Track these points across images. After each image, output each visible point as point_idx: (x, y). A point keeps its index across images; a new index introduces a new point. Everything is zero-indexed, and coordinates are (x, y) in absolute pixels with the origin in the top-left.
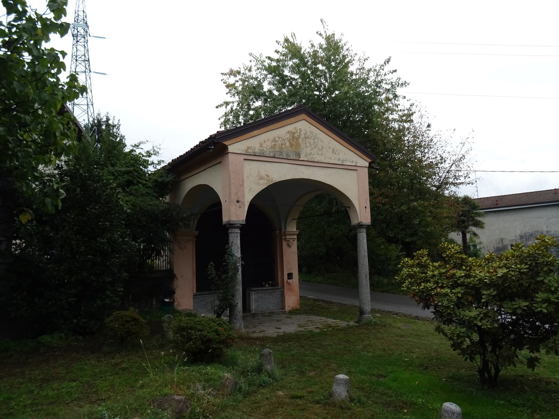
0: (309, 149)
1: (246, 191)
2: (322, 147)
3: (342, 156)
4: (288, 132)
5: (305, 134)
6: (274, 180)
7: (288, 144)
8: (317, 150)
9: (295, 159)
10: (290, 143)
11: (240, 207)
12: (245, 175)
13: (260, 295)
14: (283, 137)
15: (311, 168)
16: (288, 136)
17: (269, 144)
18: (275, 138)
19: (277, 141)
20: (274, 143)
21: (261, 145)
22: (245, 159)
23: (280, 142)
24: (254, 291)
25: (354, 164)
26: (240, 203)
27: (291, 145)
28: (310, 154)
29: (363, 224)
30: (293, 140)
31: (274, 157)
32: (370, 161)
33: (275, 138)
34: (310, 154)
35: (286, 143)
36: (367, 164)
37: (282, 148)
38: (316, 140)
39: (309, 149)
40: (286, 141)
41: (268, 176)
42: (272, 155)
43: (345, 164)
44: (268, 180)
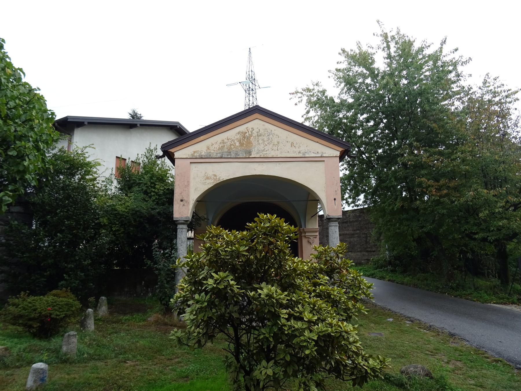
1: (192, 190)
2: (278, 143)
3: (303, 149)
4: (239, 133)
5: (258, 132)
7: (238, 144)
8: (271, 146)
9: (247, 157)
10: (240, 143)
11: (184, 205)
12: (192, 176)
14: (233, 138)
16: (238, 136)
17: (217, 146)
19: (226, 143)
20: (222, 145)
23: (229, 143)
27: (241, 144)
28: (263, 150)
32: (341, 149)
34: (263, 150)
36: (338, 154)
37: (231, 148)
38: (271, 136)
39: (262, 145)
40: (236, 141)
41: (215, 176)
42: (219, 155)
44: (215, 180)
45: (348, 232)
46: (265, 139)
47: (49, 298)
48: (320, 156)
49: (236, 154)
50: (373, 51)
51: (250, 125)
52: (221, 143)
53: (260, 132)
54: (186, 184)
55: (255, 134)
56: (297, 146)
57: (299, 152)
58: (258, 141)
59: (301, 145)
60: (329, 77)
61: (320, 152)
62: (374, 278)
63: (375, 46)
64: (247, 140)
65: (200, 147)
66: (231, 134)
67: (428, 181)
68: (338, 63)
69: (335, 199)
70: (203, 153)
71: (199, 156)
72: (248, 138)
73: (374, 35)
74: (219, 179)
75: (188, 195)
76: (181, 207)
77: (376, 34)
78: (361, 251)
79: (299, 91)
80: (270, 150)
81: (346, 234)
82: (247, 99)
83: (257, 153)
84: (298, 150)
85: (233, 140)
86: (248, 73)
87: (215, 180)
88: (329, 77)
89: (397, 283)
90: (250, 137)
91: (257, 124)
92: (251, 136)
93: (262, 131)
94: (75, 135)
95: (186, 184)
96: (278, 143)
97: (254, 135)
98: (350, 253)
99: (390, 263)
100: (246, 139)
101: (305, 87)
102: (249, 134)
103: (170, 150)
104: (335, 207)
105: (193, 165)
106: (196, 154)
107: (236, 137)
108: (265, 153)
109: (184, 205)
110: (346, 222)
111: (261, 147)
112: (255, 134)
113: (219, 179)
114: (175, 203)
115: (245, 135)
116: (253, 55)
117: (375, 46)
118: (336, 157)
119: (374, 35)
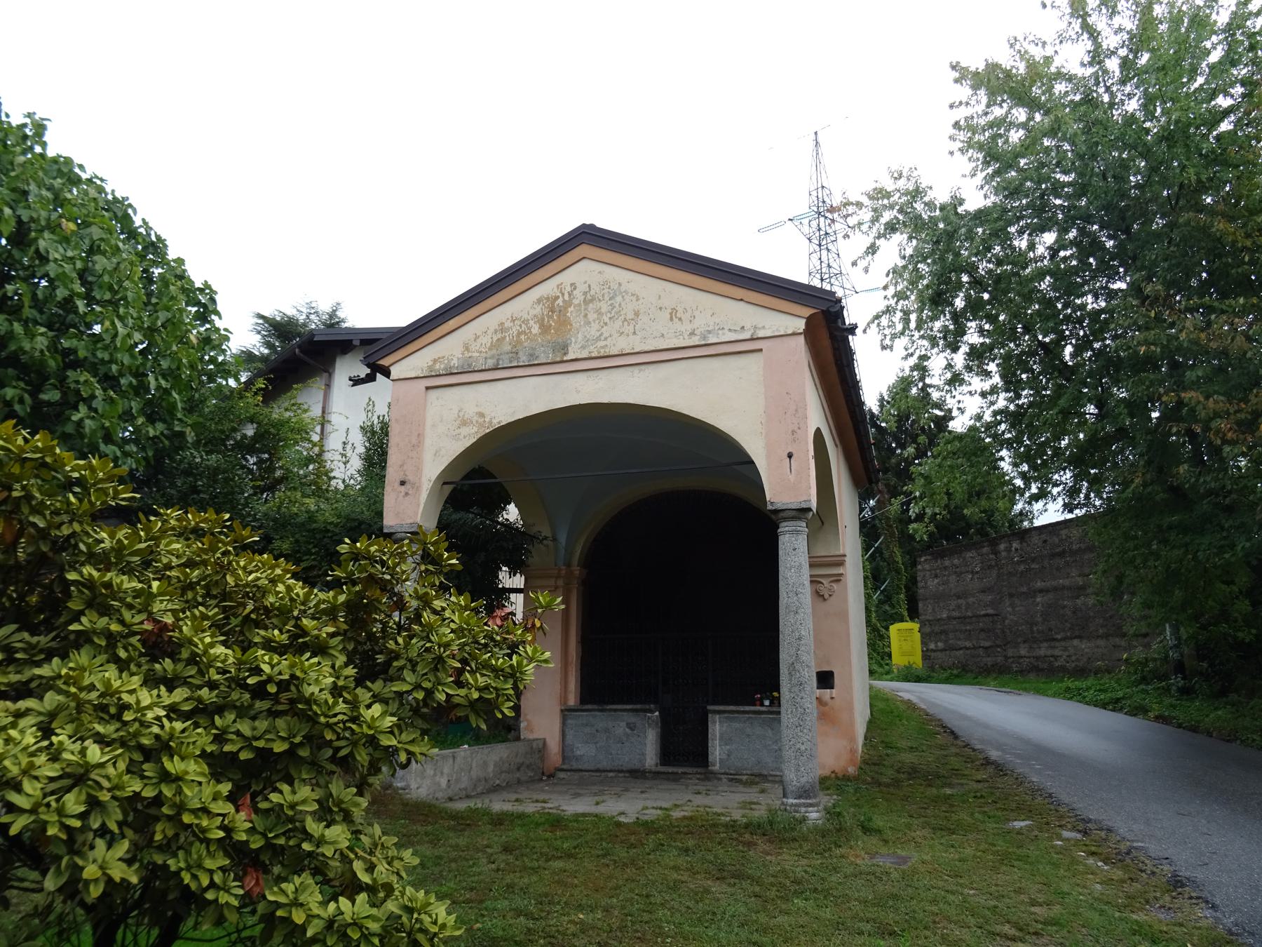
0: (595, 326)
1: (428, 456)
2: (637, 314)
3: (701, 323)
4: (539, 301)
5: (585, 293)
6: (495, 421)
7: (536, 329)
8: (618, 323)
9: (558, 361)
10: (542, 326)
11: (407, 494)
12: (429, 422)
13: (737, 725)
14: (526, 316)
15: (499, 384)
16: (538, 310)
17: (486, 340)
18: (502, 324)
19: (508, 329)
20: (499, 336)
21: (467, 349)
22: (427, 388)
23: (515, 331)
24: (719, 712)
25: (747, 335)
26: (408, 486)
27: (545, 329)
28: (598, 339)
29: (779, 506)
30: (550, 317)
31: (752, 339)
32: (808, 312)
33: (502, 324)
34: (598, 339)
35: (529, 329)
36: (800, 325)
37: (519, 342)
38: (619, 299)
39: (595, 326)
40: (531, 322)
41: (482, 415)
42: (490, 363)
43: (712, 340)
44: (481, 425)
45: (1067, 582)
46: (605, 308)
47: (389, 743)
48: (748, 336)
49: (531, 355)
50: (1049, 51)
51: (566, 278)
52: (496, 331)
53: (592, 292)
54: (414, 441)
55: (579, 296)
56: (685, 317)
57: (692, 334)
58: (586, 316)
59: (697, 313)
60: (952, 153)
61: (747, 326)
62: (1121, 710)
63: (1050, 36)
64: (559, 317)
65: (447, 348)
66: (522, 307)
67: (1207, 398)
68: (951, 106)
69: (790, 456)
70: (455, 362)
71: (445, 369)
72: (562, 311)
73: (1044, 6)
74: (491, 422)
75: (418, 470)
76: (401, 497)
77: (1049, 5)
78: (1106, 636)
79: (852, 200)
80: (615, 335)
81: (1064, 587)
82: (815, 257)
83: (583, 347)
84: (689, 327)
85: (526, 322)
86: (814, 193)
87: (481, 425)
88: (952, 153)
89: (1180, 726)
90: (566, 308)
91: (586, 273)
92: (568, 304)
93: (596, 288)
94: (337, 371)
95: (414, 441)
96: (637, 314)
97: (576, 302)
98: (1076, 642)
99: (1180, 668)
100: (556, 316)
101: (870, 187)
102: (564, 301)
103: (381, 362)
104: (792, 478)
105: (433, 394)
106: (437, 366)
107: (533, 312)
108: (602, 343)
109: (407, 494)
110: (1062, 554)
111: (593, 331)
112: (579, 296)
113: (491, 422)
114: (388, 489)
115: (553, 303)
116: (824, 148)
117: (1050, 36)
118: (794, 334)
119: (1044, 6)
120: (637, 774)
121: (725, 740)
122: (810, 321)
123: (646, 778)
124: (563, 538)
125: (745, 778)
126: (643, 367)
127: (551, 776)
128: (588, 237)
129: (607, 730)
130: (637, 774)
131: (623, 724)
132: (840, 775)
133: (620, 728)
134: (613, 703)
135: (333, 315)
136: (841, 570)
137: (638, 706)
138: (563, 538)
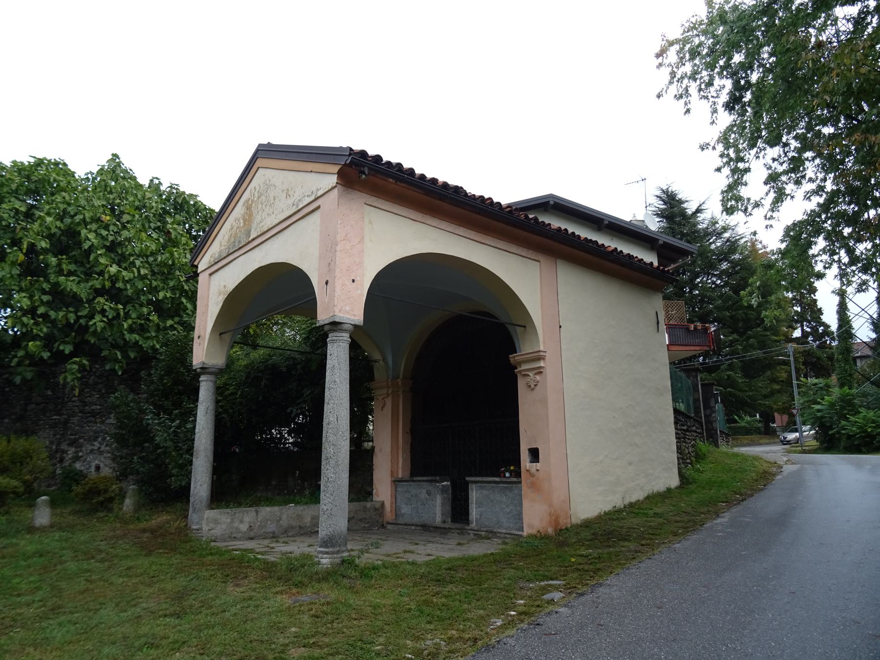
13: (485, 492)
22: (211, 275)
32: (336, 169)
36: (333, 179)
43: (301, 206)
69: (327, 283)
120: (426, 528)
121: (479, 504)
122: (341, 174)
123: (430, 531)
124: (390, 360)
125: (483, 533)
126: (278, 236)
127: (383, 526)
128: (267, 153)
129: (416, 496)
130: (426, 528)
131: (425, 491)
132: (543, 534)
133: (423, 495)
134: (476, 475)
135: (713, 218)
136: (542, 364)
137: (429, 478)
138: (390, 360)
